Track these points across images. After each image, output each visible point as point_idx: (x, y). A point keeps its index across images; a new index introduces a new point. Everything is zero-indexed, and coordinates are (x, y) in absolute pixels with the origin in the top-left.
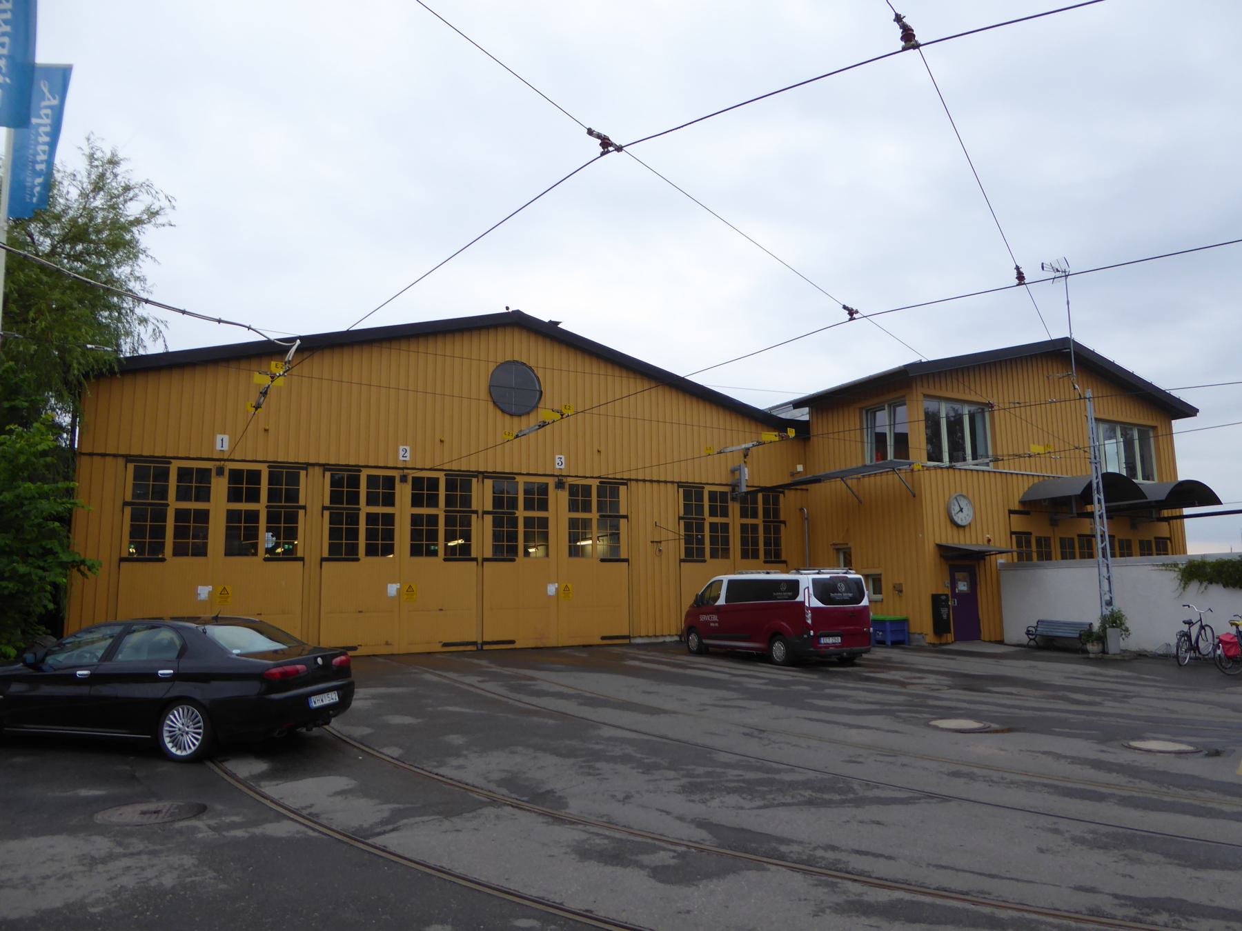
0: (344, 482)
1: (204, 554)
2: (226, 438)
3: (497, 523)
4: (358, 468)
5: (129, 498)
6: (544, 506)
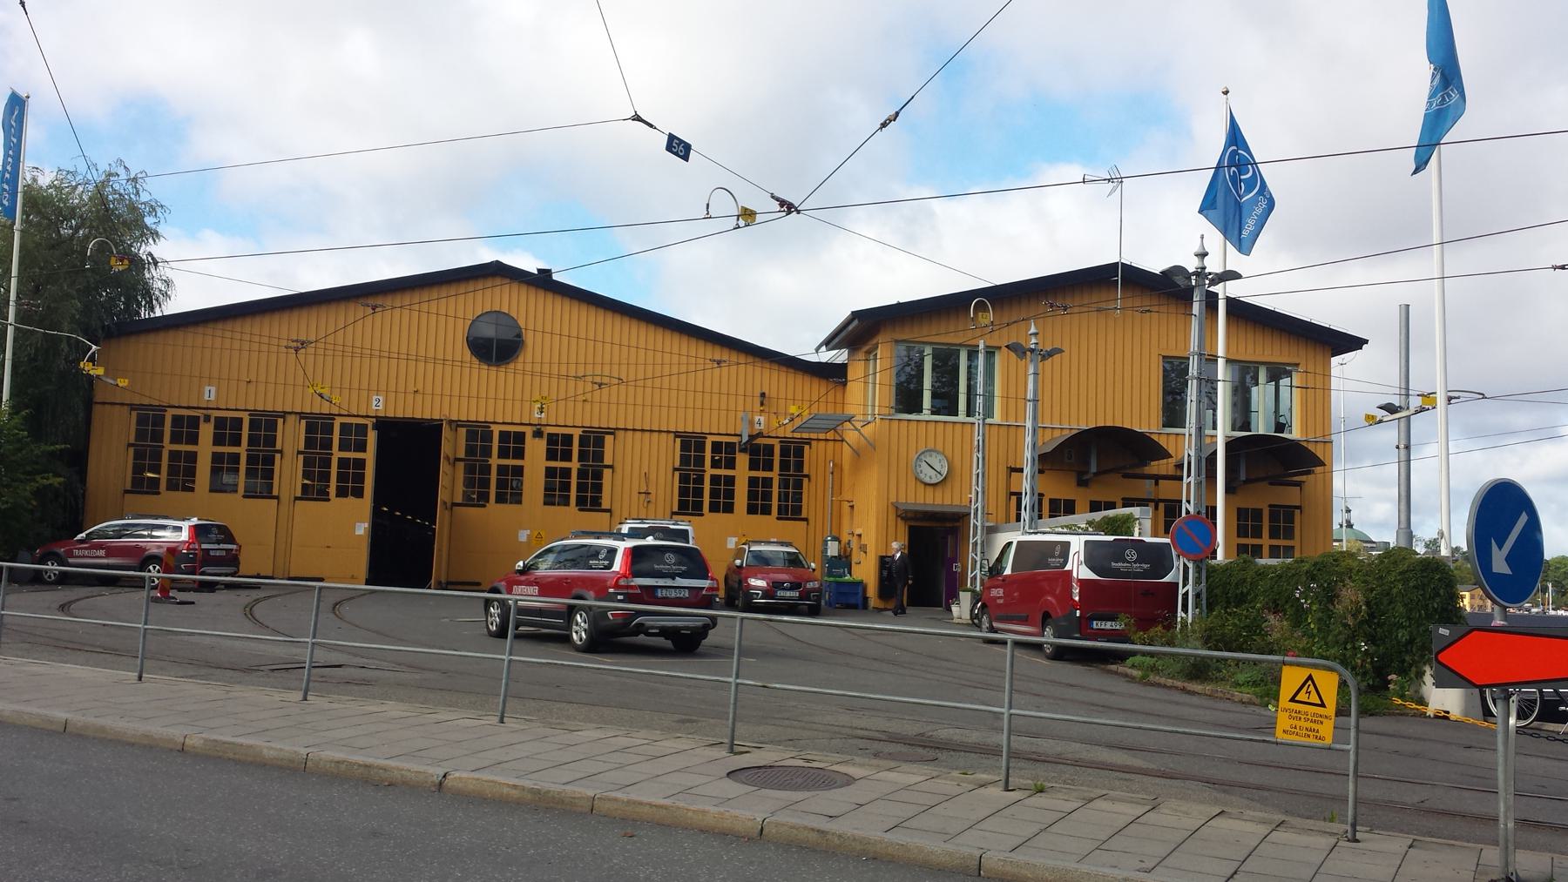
0: (318, 427)
1: (520, 502)
2: (213, 389)
3: (470, 470)
4: (163, 408)
5: (132, 441)
6: (520, 454)
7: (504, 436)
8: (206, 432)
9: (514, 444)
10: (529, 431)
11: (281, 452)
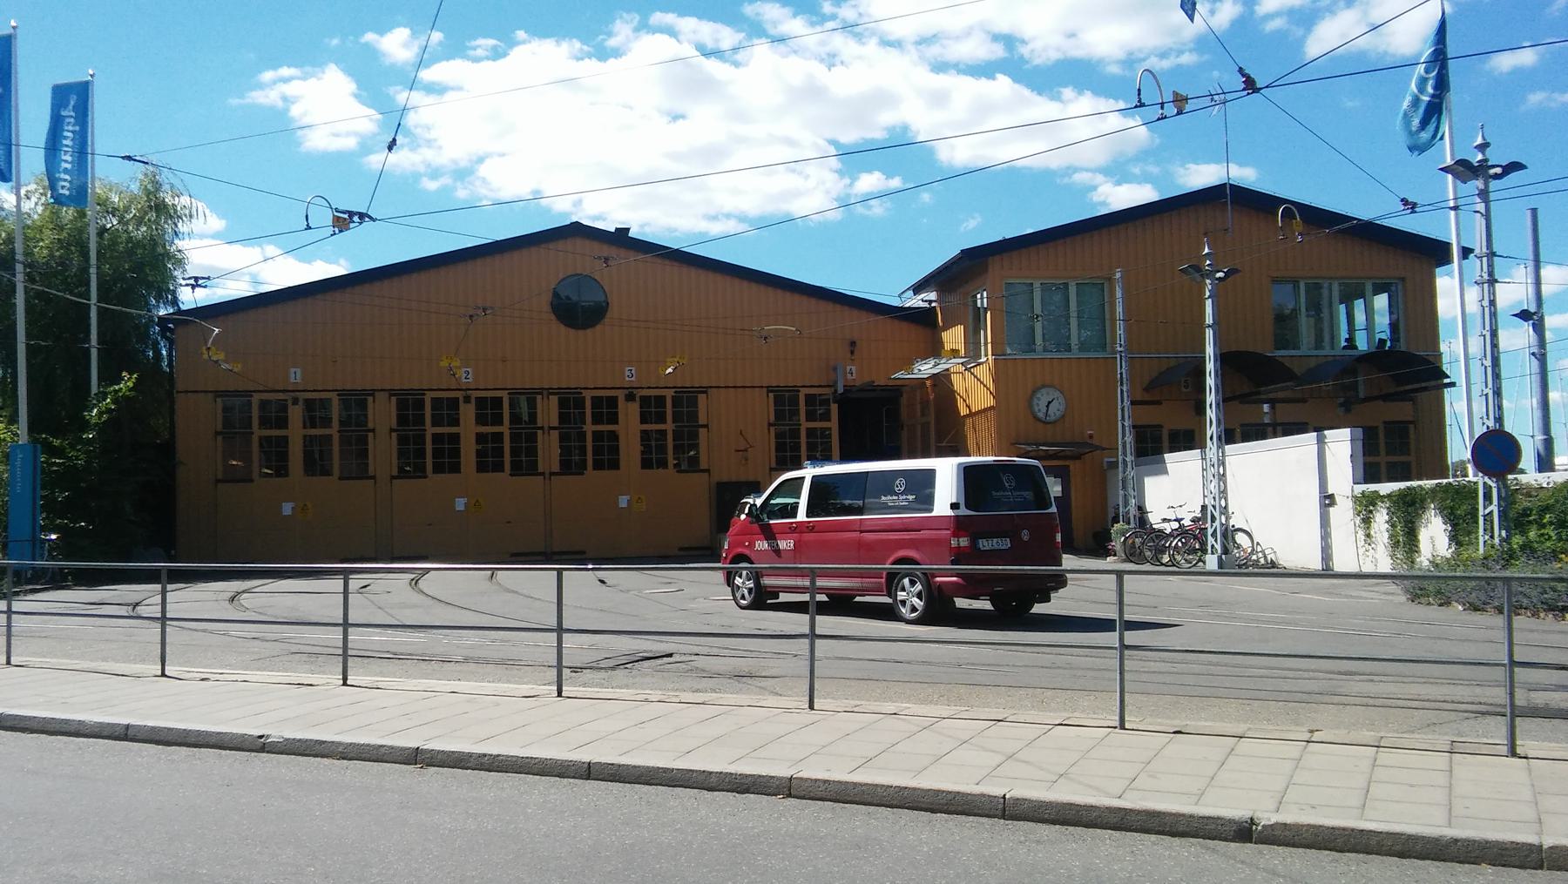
2: (299, 371)
4: (422, 392)
6: (614, 419)
7: (597, 401)
8: (468, 412)
9: (606, 409)
10: (621, 395)
11: (373, 430)
